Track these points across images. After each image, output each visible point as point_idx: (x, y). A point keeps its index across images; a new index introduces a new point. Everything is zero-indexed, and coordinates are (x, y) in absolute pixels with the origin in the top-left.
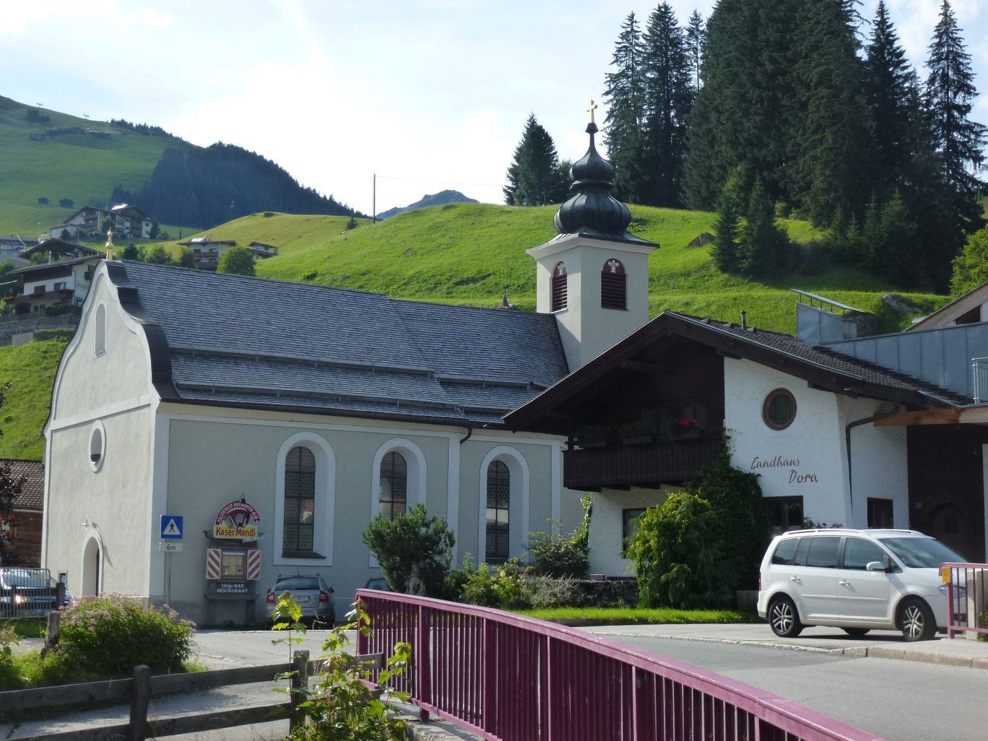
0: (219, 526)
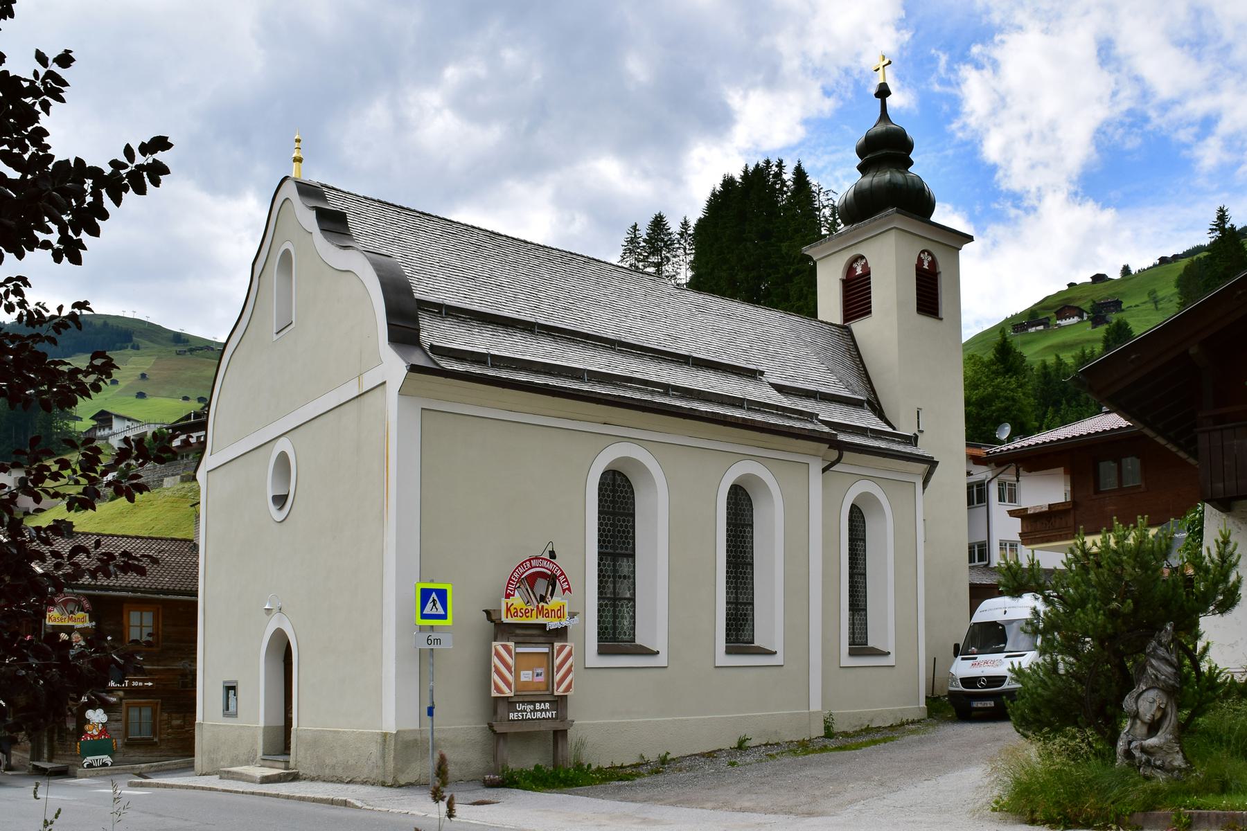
0: (510, 601)
